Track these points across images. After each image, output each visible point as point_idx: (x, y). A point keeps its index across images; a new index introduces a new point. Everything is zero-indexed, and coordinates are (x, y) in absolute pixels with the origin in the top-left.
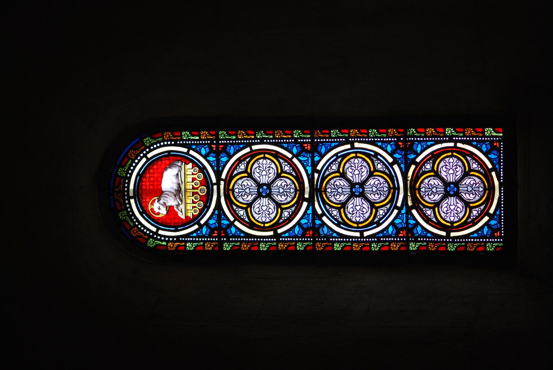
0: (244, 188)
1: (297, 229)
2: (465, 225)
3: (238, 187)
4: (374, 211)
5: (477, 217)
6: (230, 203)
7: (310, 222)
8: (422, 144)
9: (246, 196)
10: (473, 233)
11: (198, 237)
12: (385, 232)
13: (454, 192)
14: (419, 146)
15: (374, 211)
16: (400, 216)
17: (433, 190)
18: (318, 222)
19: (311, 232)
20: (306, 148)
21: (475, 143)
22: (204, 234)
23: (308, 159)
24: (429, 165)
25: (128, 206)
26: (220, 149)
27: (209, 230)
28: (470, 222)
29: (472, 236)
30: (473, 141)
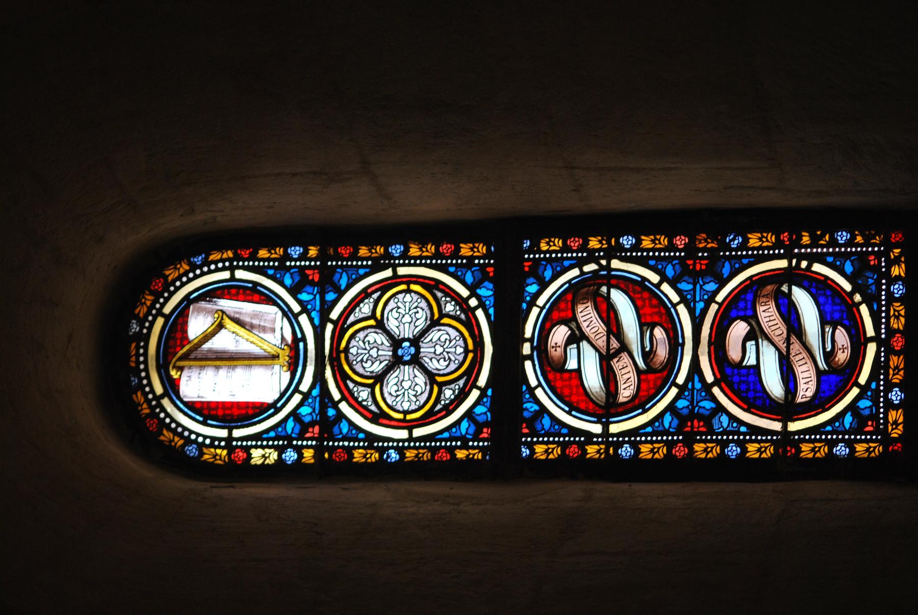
0: (368, 350)
1: (290, 424)
2: (430, 417)
3: (355, 344)
4: (436, 389)
5: (452, 402)
6: (342, 378)
7: (317, 411)
8: (350, 273)
9: (443, 339)
10: (267, 431)
11: (654, 433)
12: (280, 429)
13: (403, 356)
14: (345, 276)
15: (436, 389)
16: (310, 400)
17: (371, 352)
18: (331, 412)
19: (317, 429)
20: (311, 278)
21: (452, 269)
22: (344, 275)
23: (315, 298)
24: (452, 308)
25: (145, 382)
26: (527, 269)
27: (298, 427)
28: (440, 411)
29: (265, 436)
30: (269, 267)
